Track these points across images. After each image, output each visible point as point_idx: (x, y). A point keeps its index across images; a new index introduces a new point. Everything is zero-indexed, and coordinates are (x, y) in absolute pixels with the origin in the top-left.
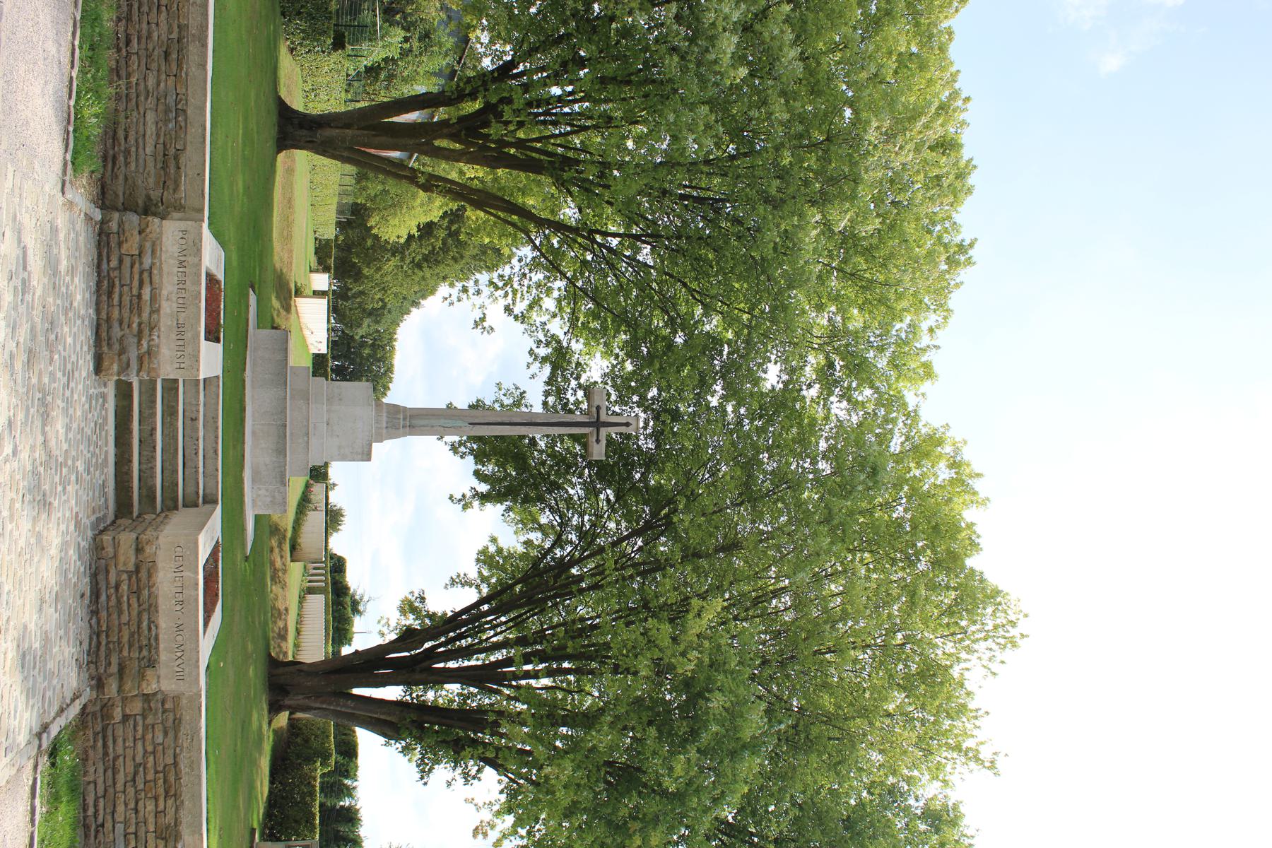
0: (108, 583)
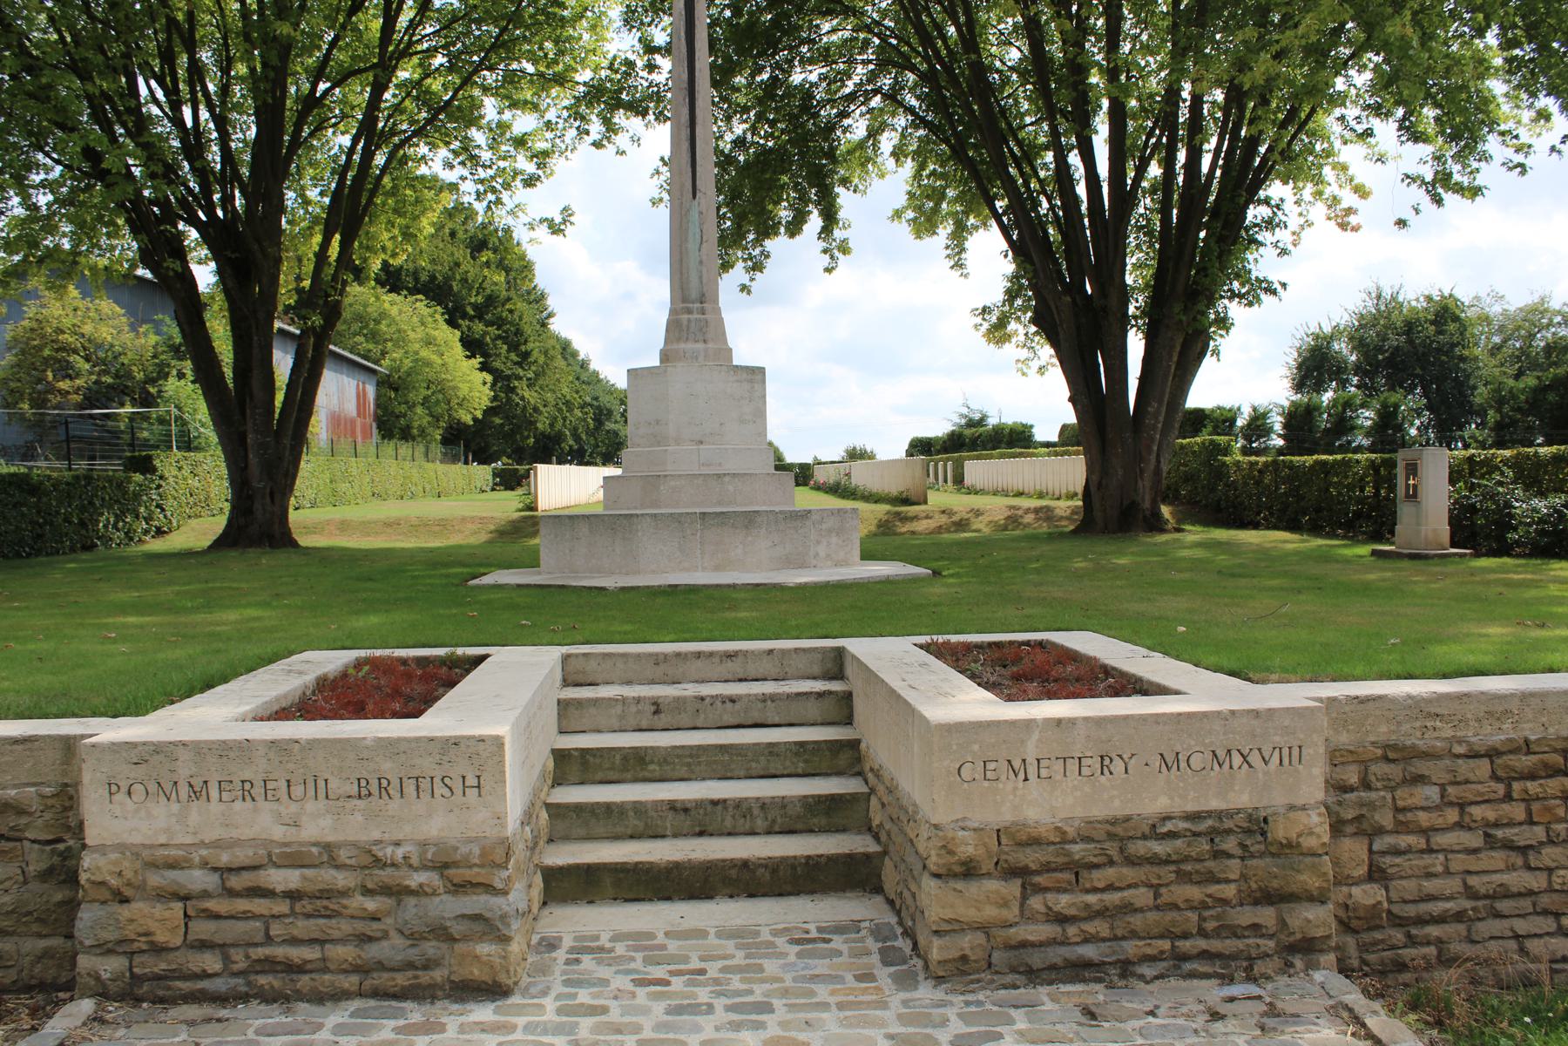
0: (1053, 942)
